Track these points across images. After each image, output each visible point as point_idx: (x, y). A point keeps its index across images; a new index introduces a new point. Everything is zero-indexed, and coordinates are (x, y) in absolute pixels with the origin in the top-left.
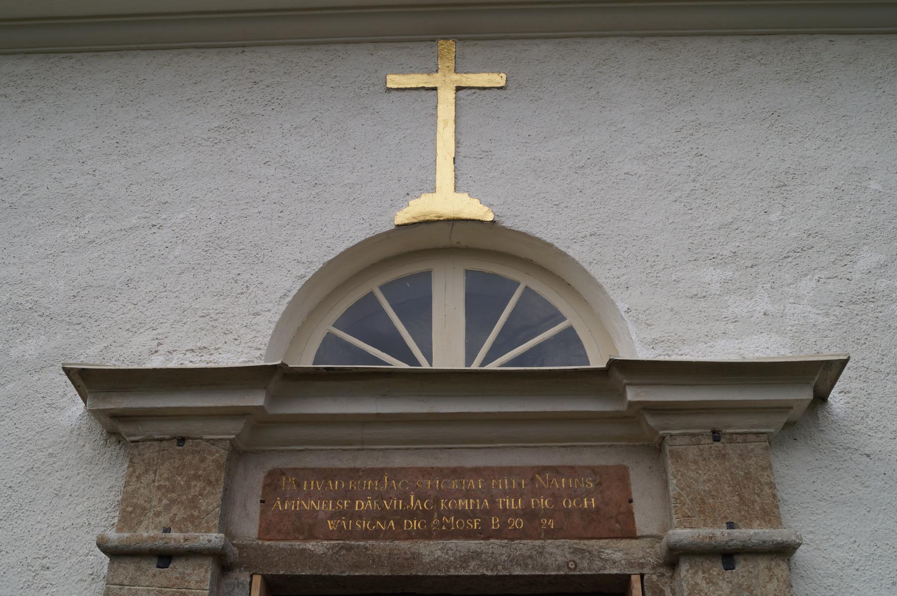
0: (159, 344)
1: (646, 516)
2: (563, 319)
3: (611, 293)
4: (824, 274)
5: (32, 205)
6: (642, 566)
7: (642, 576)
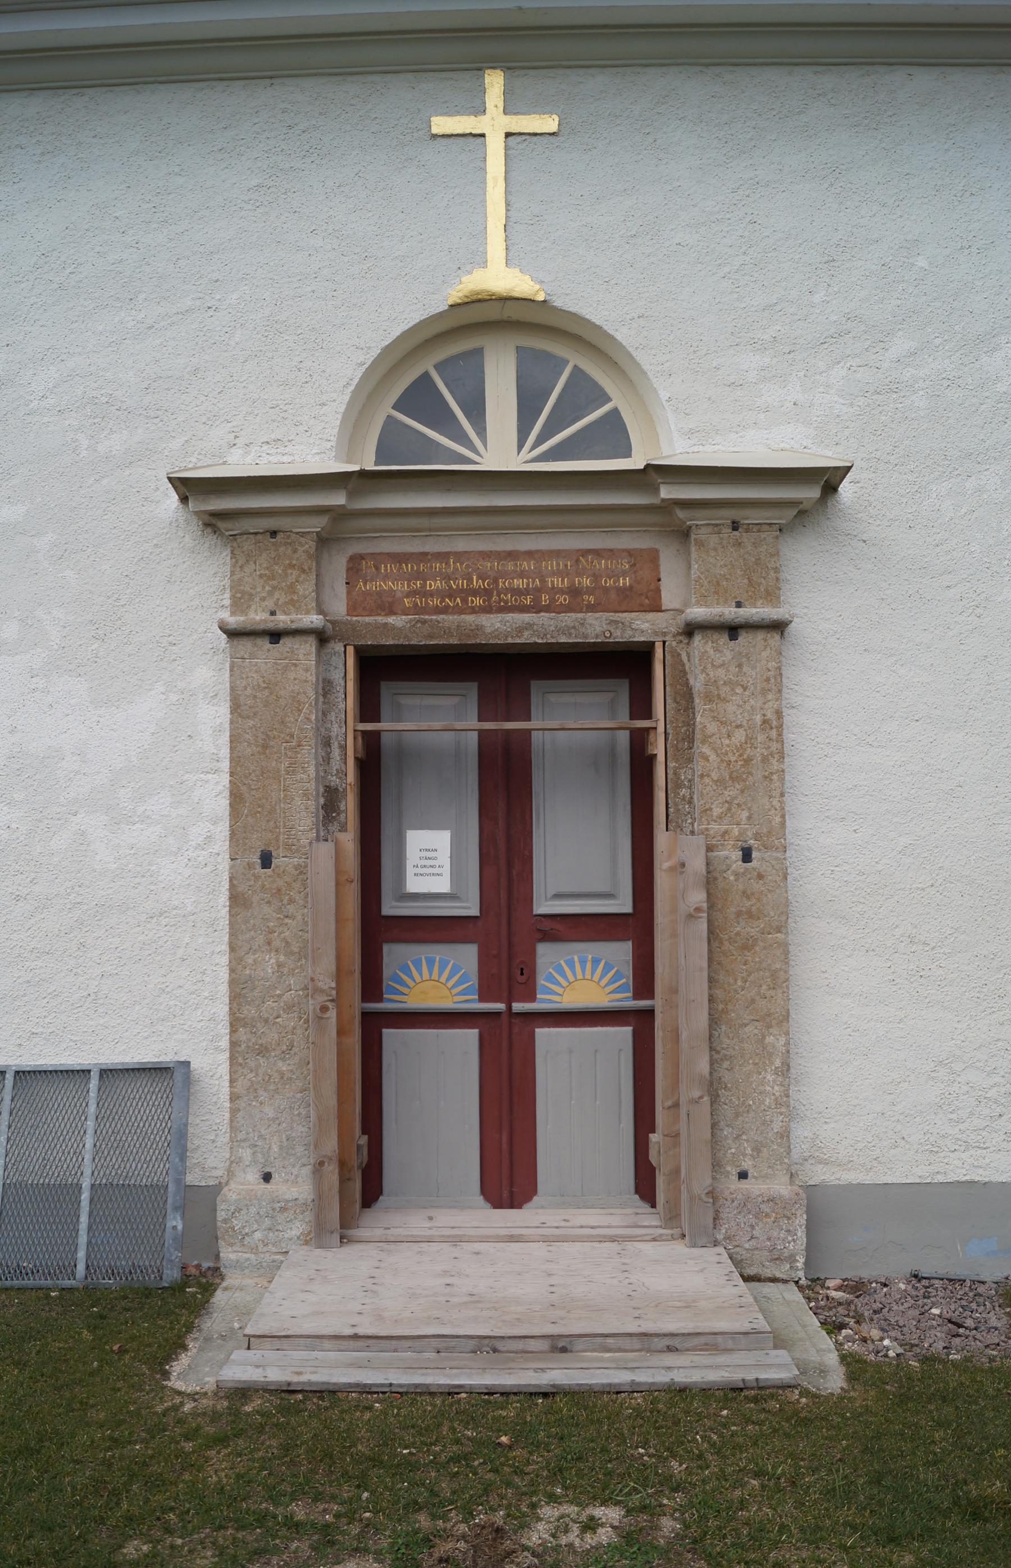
0: (236, 437)
1: (670, 595)
2: (609, 400)
3: (654, 380)
4: (858, 361)
5: (81, 285)
6: (665, 634)
7: (664, 642)
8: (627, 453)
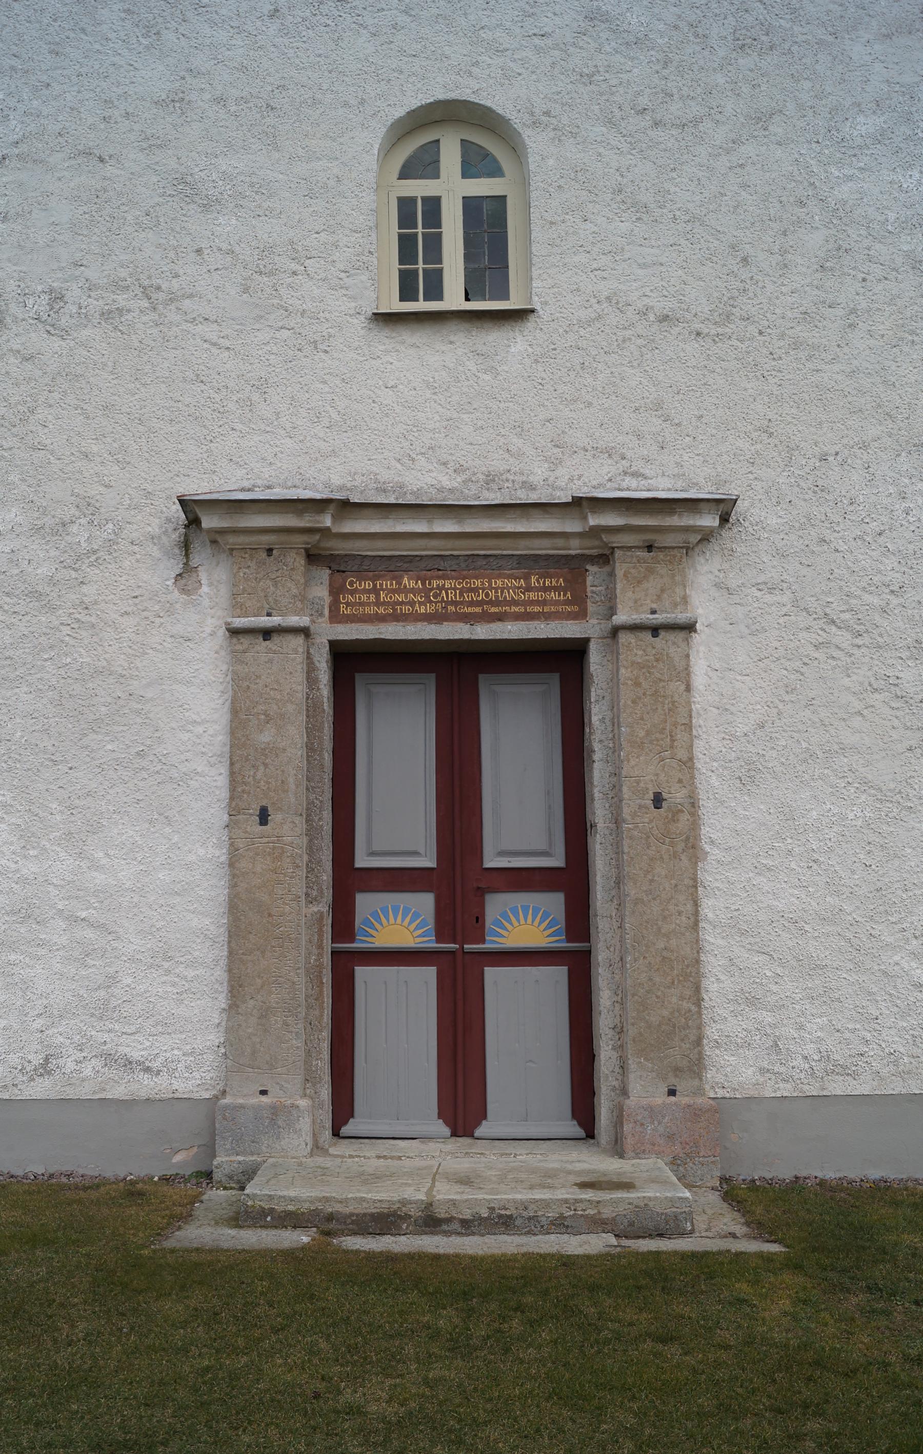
8: (506, 296)
